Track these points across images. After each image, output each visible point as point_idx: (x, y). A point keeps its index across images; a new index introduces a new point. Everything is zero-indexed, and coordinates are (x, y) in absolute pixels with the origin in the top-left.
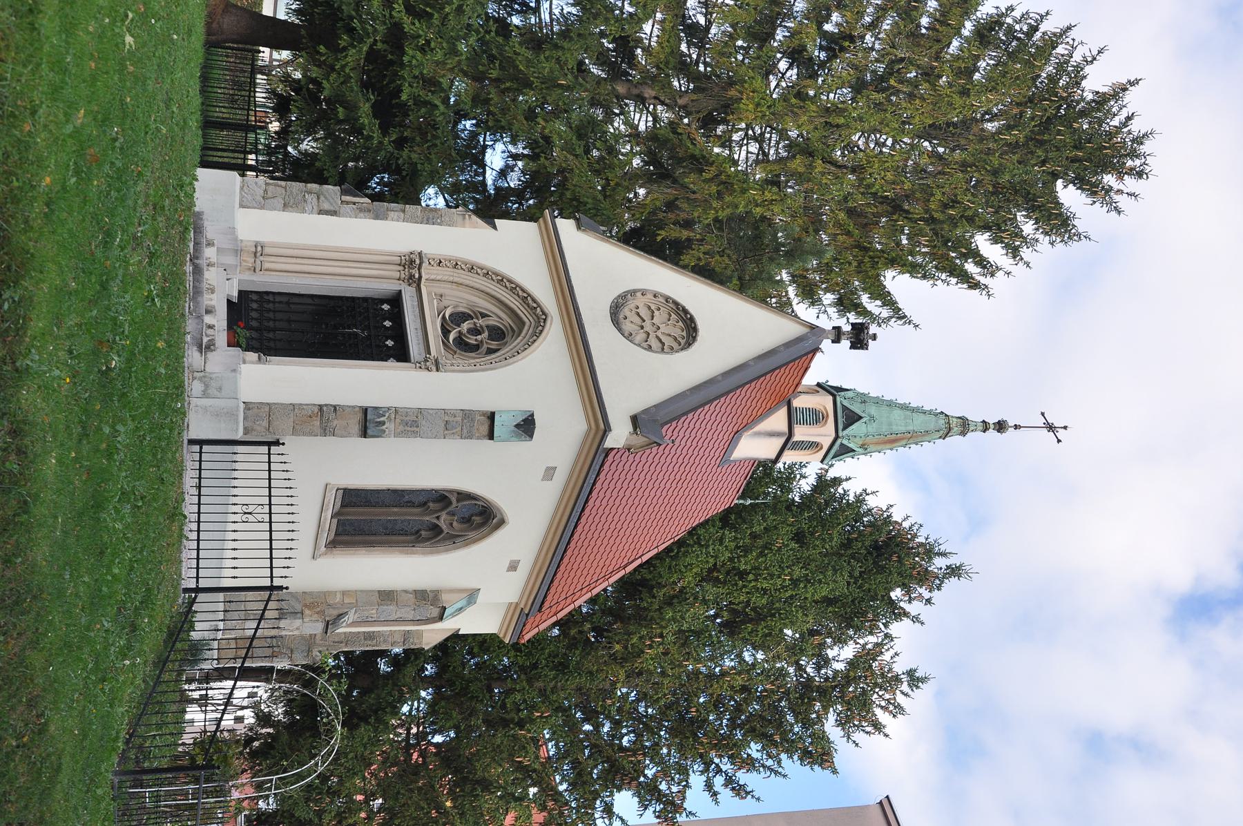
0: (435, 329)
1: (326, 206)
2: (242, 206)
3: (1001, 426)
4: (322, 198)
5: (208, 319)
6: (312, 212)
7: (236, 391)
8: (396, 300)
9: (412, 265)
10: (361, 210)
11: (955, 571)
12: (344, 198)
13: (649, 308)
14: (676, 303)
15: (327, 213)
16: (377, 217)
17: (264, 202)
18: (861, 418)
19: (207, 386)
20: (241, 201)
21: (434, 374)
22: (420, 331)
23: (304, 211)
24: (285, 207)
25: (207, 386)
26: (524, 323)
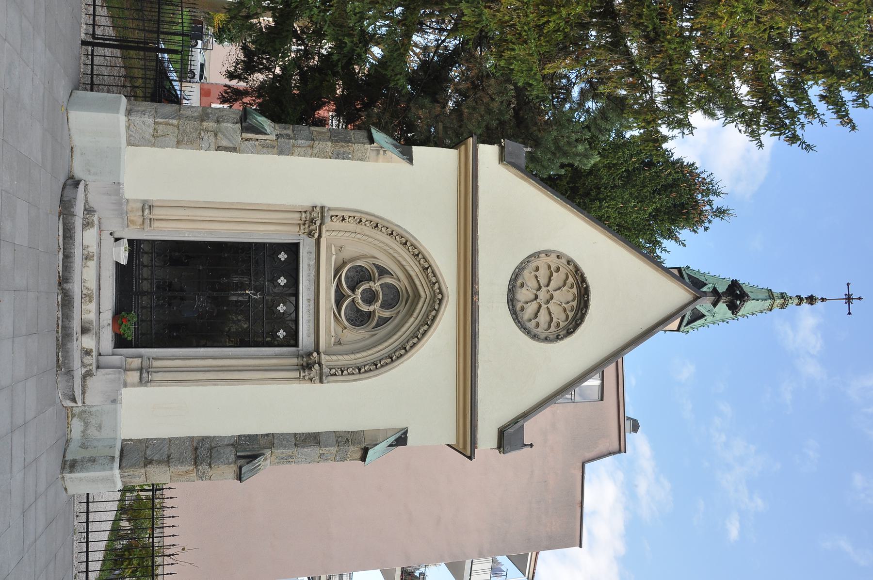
0: (328, 299)
1: (224, 143)
2: (129, 144)
3: (811, 300)
4: (220, 136)
5: (88, 342)
6: (208, 149)
7: (115, 430)
8: (293, 249)
9: (314, 219)
10: (264, 146)
11: (720, 213)
12: (245, 135)
13: (549, 267)
14: (577, 269)
15: (226, 149)
16: (281, 153)
17: (156, 140)
18: (703, 316)
19: (86, 425)
20: (129, 136)
21: (318, 385)
22: (312, 303)
23: (200, 148)
24: (179, 144)
25: (86, 425)
26: (419, 296)
